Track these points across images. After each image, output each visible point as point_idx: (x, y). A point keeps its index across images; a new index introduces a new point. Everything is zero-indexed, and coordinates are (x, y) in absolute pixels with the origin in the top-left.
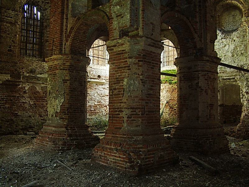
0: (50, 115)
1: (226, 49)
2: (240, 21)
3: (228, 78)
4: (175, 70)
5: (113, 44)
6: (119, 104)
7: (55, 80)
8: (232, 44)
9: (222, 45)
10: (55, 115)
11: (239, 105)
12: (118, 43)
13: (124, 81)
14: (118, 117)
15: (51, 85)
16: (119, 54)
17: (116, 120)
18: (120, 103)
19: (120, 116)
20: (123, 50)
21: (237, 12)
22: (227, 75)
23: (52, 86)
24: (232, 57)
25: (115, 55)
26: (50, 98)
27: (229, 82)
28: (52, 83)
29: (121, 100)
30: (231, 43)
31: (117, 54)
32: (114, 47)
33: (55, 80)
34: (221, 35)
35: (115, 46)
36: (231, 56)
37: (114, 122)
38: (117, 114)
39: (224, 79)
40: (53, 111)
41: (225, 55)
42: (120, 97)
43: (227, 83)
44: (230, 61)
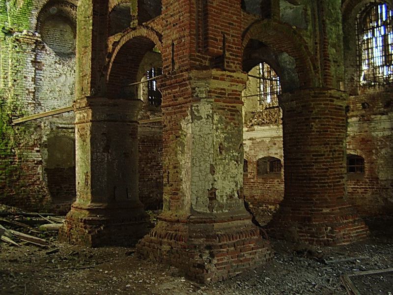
0: (222, 196)
1: (62, 81)
2: (71, 43)
3: (66, 126)
4: (38, 104)
5: (337, 96)
6: (340, 169)
7: (235, 124)
8: (71, 75)
9: (56, 74)
10: (238, 194)
11: (64, 169)
12: (342, 96)
13: (343, 142)
14: (339, 185)
15: (225, 131)
16: (336, 108)
17: (338, 189)
18: (341, 167)
19: (341, 183)
20: (341, 106)
21: (68, 28)
22: (64, 122)
23: (228, 133)
24: (70, 96)
25: (333, 108)
26: (222, 159)
27: (65, 132)
28: (229, 127)
29: (341, 164)
30: (70, 74)
31: (336, 108)
32: (337, 99)
33: (235, 124)
34: (54, 56)
35: (338, 98)
36: (69, 93)
37: (335, 191)
38: (337, 182)
39: (58, 128)
40: (233, 186)
41: (60, 91)
42: (339, 161)
43: (62, 133)
44: (67, 100)
